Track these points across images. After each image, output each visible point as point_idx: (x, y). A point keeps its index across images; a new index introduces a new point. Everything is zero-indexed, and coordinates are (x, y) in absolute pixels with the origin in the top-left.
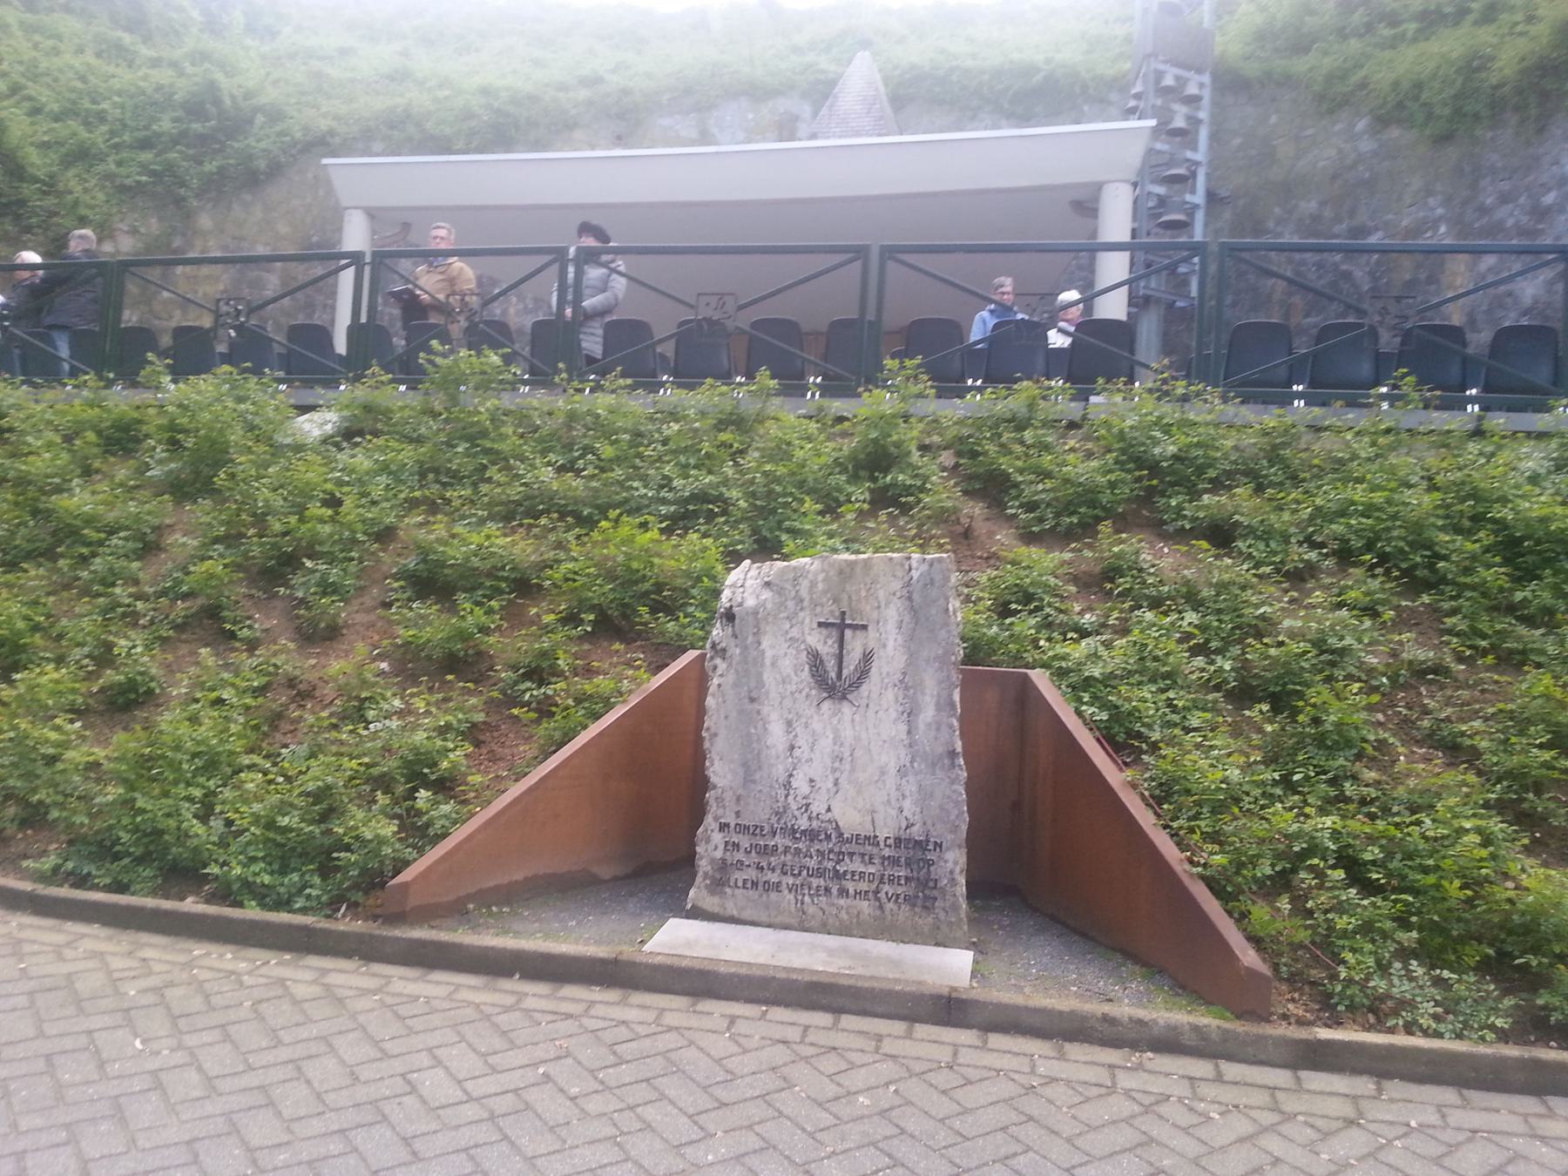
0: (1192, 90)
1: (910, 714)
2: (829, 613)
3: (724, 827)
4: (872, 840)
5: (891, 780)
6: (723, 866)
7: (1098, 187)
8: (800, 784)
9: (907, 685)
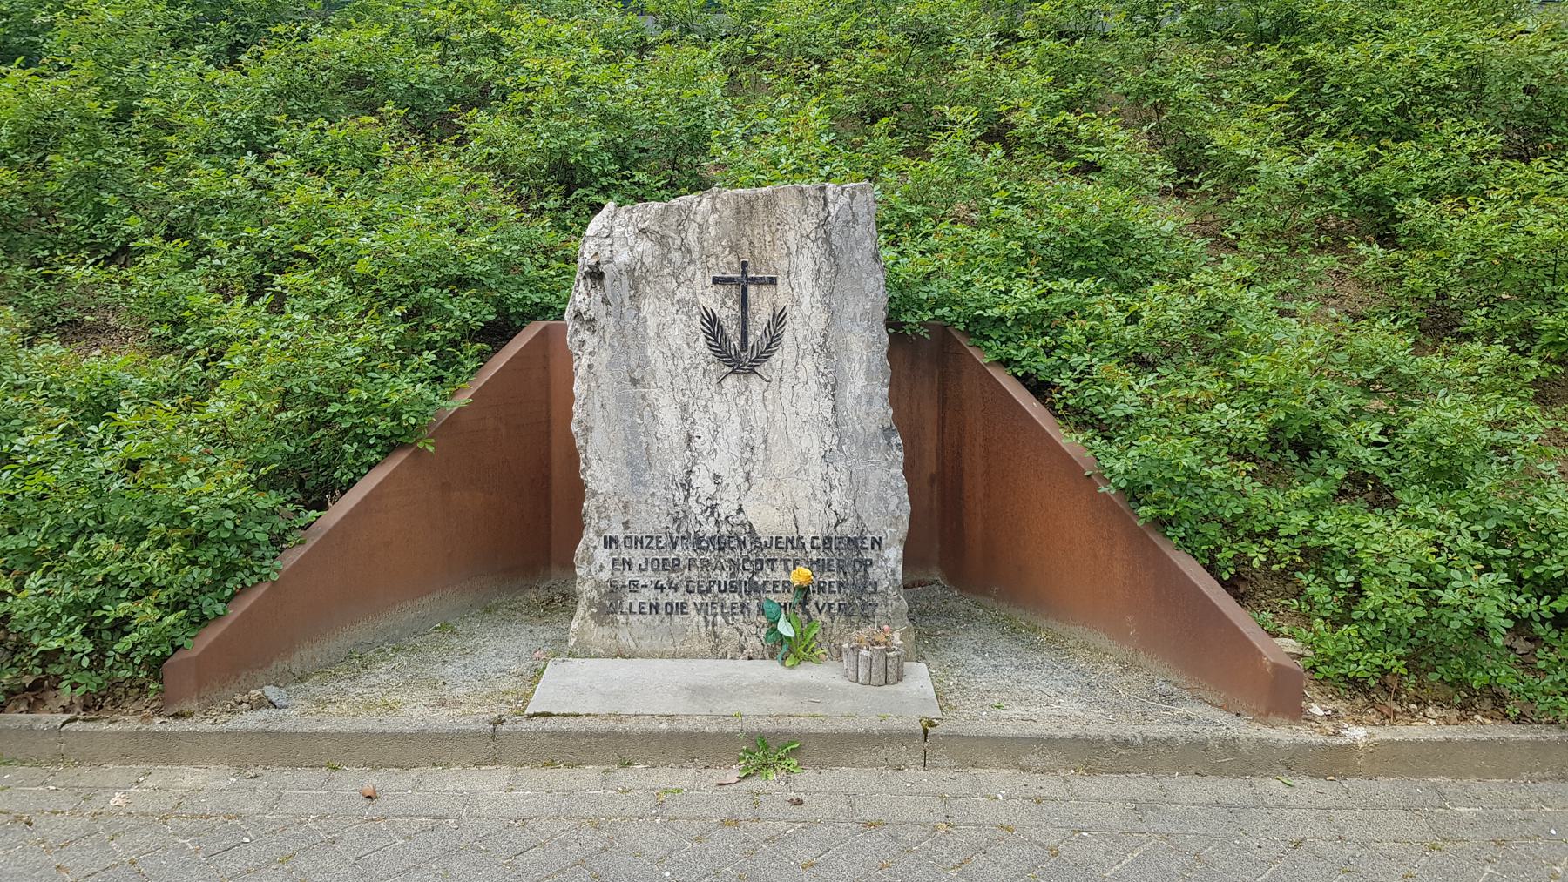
1: (833, 387)
2: (726, 264)
3: (609, 542)
4: (796, 542)
5: (815, 467)
9: (827, 348)
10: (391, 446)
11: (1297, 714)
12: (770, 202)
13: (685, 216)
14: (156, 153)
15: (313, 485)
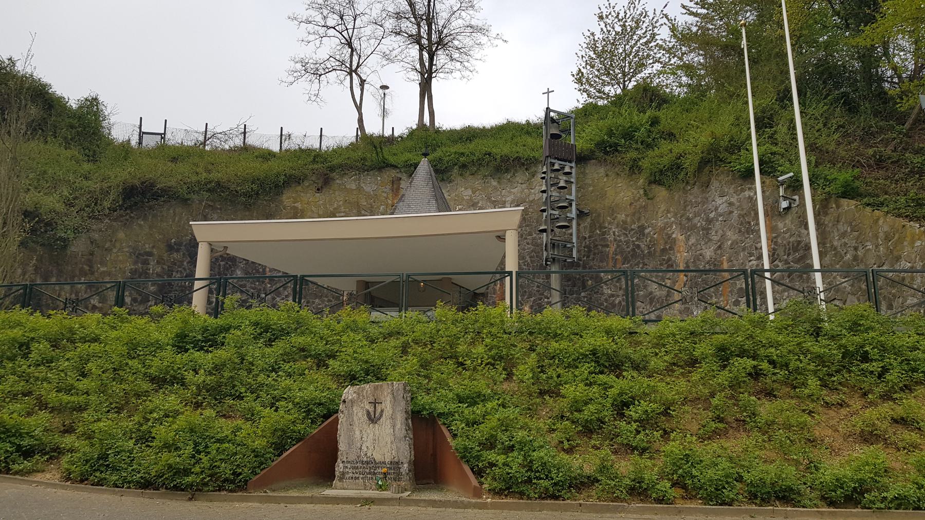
0: (567, 170)
1: (394, 426)
2: (371, 399)
3: (343, 462)
4: (384, 463)
5: (389, 445)
6: (343, 474)
7: (505, 231)
8: (364, 448)
9: (393, 418)
10: (299, 440)
11: (480, 497)
12: (381, 386)
13: (364, 389)
14: (250, 371)
15: (280, 448)
